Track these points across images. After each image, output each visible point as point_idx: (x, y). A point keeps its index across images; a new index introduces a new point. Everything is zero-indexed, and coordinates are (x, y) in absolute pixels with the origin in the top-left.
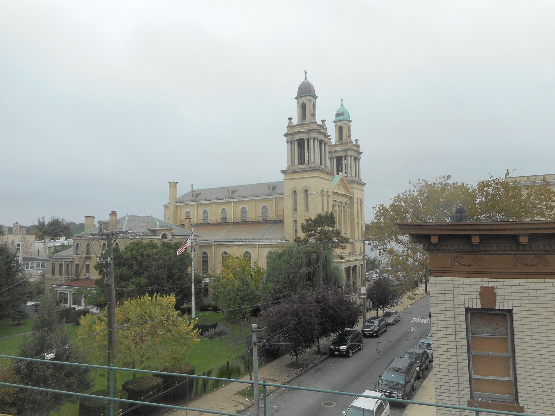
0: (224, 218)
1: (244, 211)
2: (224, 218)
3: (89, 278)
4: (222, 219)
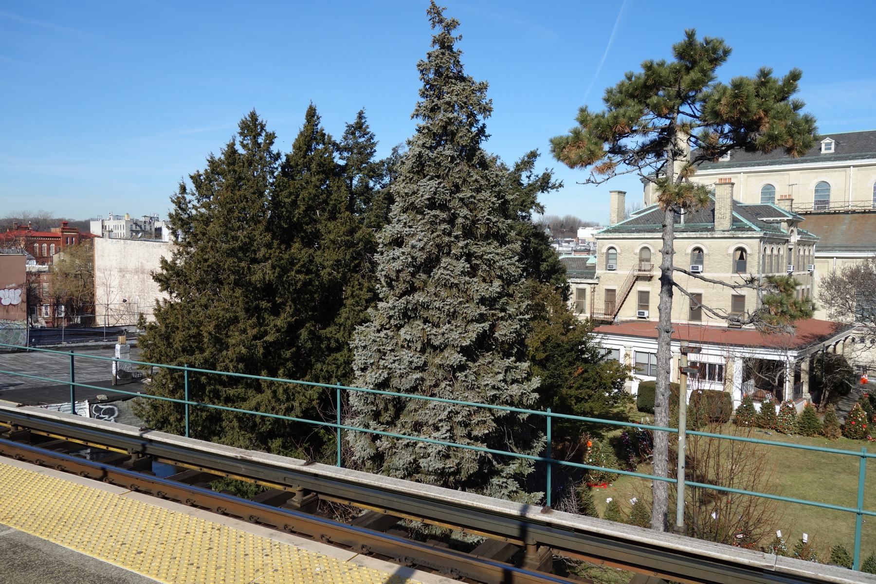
0: (822, 200)
1: (823, 189)
2: (822, 200)
3: (648, 319)
4: (816, 203)
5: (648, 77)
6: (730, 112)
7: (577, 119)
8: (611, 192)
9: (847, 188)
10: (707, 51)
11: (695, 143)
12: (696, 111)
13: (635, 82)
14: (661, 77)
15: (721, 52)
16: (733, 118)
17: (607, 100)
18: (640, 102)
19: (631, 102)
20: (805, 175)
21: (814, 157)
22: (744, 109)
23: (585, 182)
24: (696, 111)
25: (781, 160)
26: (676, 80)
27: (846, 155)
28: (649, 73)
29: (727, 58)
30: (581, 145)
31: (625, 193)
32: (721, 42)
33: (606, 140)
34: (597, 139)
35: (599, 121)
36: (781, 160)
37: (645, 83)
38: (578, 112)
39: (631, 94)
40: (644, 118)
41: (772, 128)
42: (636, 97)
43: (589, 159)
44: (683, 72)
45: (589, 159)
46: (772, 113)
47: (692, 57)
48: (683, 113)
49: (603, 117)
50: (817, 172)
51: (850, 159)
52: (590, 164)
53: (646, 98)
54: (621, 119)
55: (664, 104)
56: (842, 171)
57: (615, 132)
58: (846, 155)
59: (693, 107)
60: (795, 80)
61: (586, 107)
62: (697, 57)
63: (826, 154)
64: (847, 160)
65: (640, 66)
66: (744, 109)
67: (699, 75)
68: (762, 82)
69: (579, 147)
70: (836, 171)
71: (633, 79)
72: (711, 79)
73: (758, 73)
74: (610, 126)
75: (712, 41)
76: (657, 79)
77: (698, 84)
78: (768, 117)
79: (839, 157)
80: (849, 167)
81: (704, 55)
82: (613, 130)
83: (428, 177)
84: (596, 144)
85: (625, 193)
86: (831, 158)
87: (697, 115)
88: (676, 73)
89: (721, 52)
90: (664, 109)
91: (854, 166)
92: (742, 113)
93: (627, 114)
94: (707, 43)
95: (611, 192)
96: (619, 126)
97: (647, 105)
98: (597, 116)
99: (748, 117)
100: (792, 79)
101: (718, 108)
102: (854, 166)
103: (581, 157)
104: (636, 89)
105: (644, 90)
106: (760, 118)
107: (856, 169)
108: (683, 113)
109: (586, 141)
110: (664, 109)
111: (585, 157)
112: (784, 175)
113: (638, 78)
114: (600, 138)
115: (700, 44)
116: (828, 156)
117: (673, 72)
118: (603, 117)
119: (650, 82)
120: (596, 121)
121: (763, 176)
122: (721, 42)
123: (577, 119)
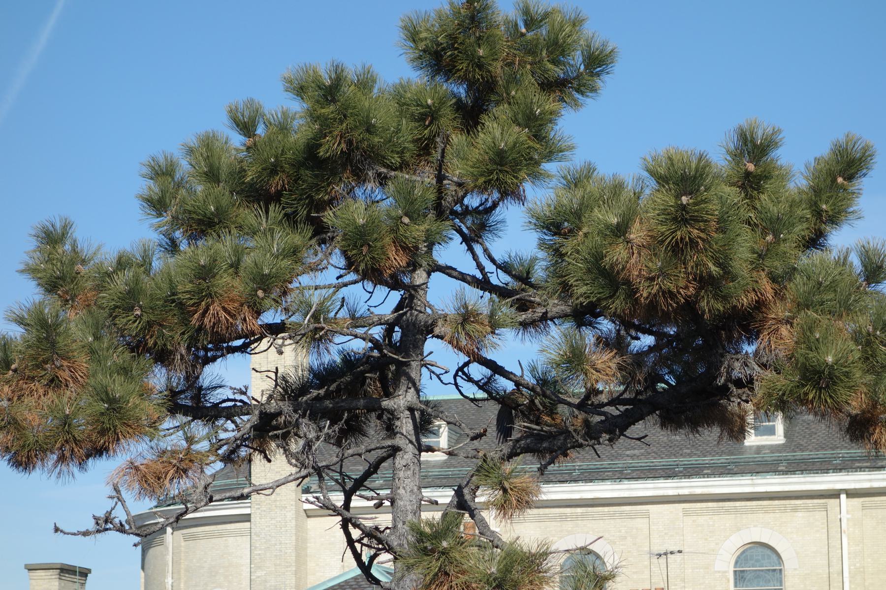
5: (325, 125)
6: (662, 273)
7: (31, 271)
8: (31, 568)
9: (836, 568)
10: (531, 49)
11: (483, 386)
12: (489, 267)
13: (270, 141)
14: (370, 129)
15: (577, 59)
16: (672, 295)
17: (157, 205)
18: (291, 219)
19: (248, 215)
20: (701, 520)
21: (723, 459)
22: (713, 268)
23: (91, 525)
24: (489, 267)
25: (620, 463)
26: (425, 148)
27: (821, 454)
28: (329, 110)
29: (599, 83)
30: (65, 375)
31: (84, 573)
32: (577, 23)
33: (163, 357)
34: (128, 355)
35: (137, 281)
36: (620, 463)
37: (312, 148)
38: (32, 244)
39: (251, 185)
40: (305, 280)
41: (806, 340)
42: (277, 197)
43: (103, 432)
44: (447, 120)
45: (103, 432)
46: (797, 286)
47: (480, 66)
48: (447, 270)
49: (145, 263)
50: (736, 510)
51: (838, 469)
52: (99, 451)
53: (321, 206)
54: (224, 280)
55: (394, 230)
56: (814, 509)
57: (200, 329)
58: (821, 454)
59: (478, 249)
60: (850, 178)
61: (67, 227)
62: (497, 68)
63: (759, 449)
64: (826, 471)
65: (280, 86)
66: (713, 268)
67: (519, 134)
68: (748, 174)
69: (54, 383)
70: (795, 509)
71: (260, 130)
72: (552, 152)
73: (732, 142)
74: (181, 305)
75: (546, 15)
76: (357, 135)
77: (515, 167)
78: (783, 299)
79: (803, 461)
80: (835, 495)
81: (522, 64)
82: (194, 320)
83: (787, 392)
84: (124, 371)
85: (84, 573)
86: (779, 461)
87: (494, 280)
88: (422, 118)
89: (577, 59)
90: (392, 253)
91: (851, 494)
92: (705, 282)
93: (247, 261)
94: (531, 22)
95: (31, 568)
96: (215, 308)
97: (321, 232)
98: (122, 263)
99: (725, 298)
100: (842, 173)
101: (618, 254)
102: (851, 494)
103: (66, 422)
104: (274, 170)
105: (306, 174)
106: (760, 305)
107: (857, 502)
108: (447, 270)
109: (83, 361)
110: (392, 253)
111: (82, 426)
112: (631, 516)
113: (283, 128)
114: (137, 347)
115: (507, 22)
116: (768, 456)
117: (413, 118)
118: (145, 263)
119: (331, 147)
120: (121, 283)
121: (563, 518)
122: (577, 23)
123: (31, 271)
